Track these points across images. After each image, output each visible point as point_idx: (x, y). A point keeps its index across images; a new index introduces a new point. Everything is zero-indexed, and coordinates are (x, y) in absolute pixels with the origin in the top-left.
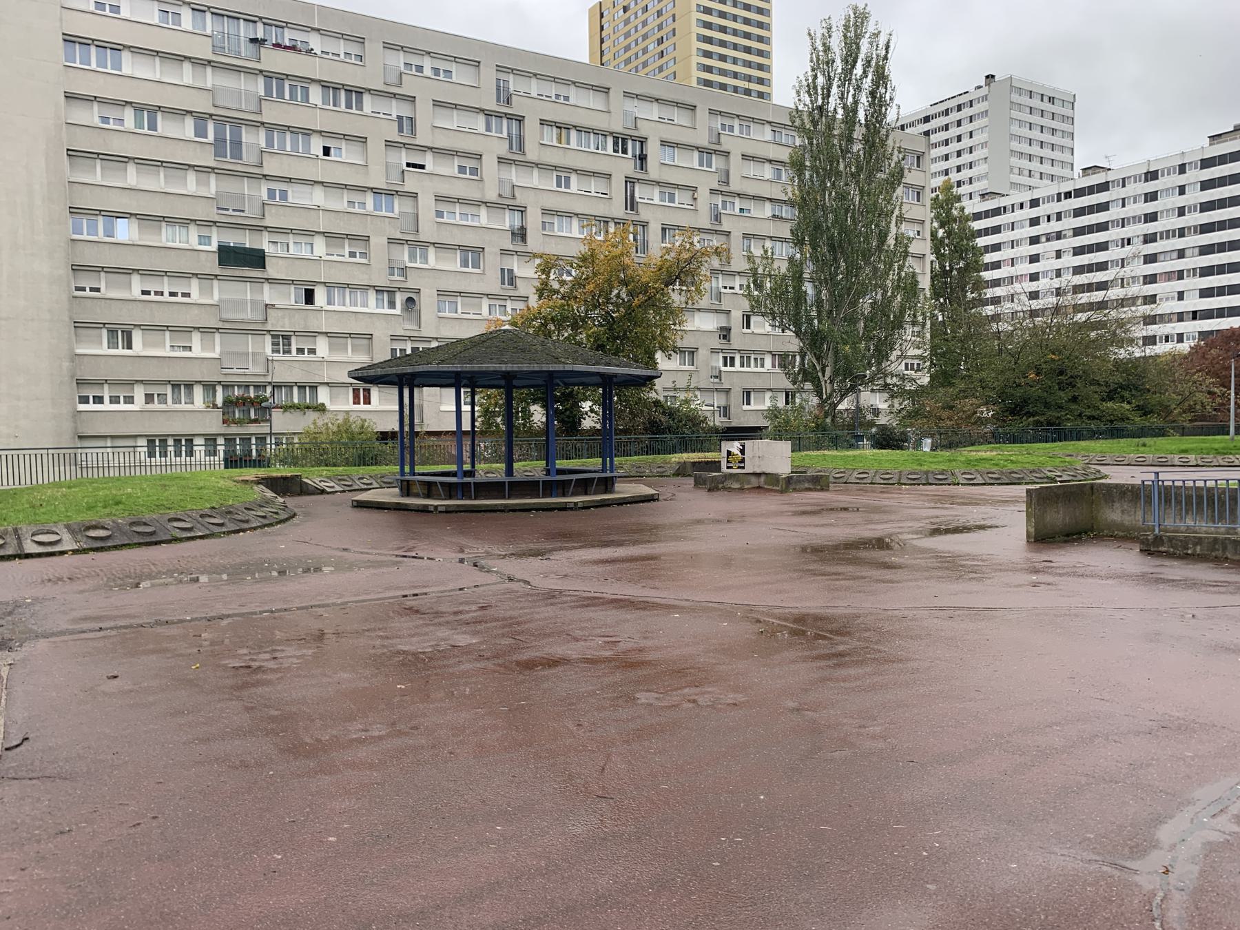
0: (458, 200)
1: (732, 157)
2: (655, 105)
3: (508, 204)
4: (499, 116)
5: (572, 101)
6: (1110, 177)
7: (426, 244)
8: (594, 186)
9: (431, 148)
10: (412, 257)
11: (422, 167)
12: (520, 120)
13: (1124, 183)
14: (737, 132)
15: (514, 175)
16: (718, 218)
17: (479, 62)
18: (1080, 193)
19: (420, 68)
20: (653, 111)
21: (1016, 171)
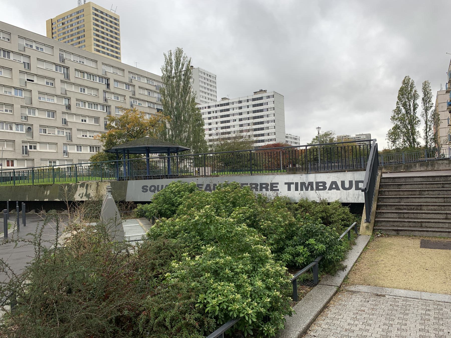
0: (47, 94)
1: (136, 87)
2: (112, 68)
3: (64, 96)
4: (60, 66)
5: (85, 64)
6: (230, 101)
7: (34, 109)
8: (93, 92)
9: (36, 75)
10: (29, 113)
11: (33, 81)
12: (68, 68)
13: (233, 103)
14: (137, 79)
15: (66, 87)
16: (132, 106)
17: (53, 47)
18: (222, 105)
19: (31, 46)
20: (111, 70)
21: (202, 97)
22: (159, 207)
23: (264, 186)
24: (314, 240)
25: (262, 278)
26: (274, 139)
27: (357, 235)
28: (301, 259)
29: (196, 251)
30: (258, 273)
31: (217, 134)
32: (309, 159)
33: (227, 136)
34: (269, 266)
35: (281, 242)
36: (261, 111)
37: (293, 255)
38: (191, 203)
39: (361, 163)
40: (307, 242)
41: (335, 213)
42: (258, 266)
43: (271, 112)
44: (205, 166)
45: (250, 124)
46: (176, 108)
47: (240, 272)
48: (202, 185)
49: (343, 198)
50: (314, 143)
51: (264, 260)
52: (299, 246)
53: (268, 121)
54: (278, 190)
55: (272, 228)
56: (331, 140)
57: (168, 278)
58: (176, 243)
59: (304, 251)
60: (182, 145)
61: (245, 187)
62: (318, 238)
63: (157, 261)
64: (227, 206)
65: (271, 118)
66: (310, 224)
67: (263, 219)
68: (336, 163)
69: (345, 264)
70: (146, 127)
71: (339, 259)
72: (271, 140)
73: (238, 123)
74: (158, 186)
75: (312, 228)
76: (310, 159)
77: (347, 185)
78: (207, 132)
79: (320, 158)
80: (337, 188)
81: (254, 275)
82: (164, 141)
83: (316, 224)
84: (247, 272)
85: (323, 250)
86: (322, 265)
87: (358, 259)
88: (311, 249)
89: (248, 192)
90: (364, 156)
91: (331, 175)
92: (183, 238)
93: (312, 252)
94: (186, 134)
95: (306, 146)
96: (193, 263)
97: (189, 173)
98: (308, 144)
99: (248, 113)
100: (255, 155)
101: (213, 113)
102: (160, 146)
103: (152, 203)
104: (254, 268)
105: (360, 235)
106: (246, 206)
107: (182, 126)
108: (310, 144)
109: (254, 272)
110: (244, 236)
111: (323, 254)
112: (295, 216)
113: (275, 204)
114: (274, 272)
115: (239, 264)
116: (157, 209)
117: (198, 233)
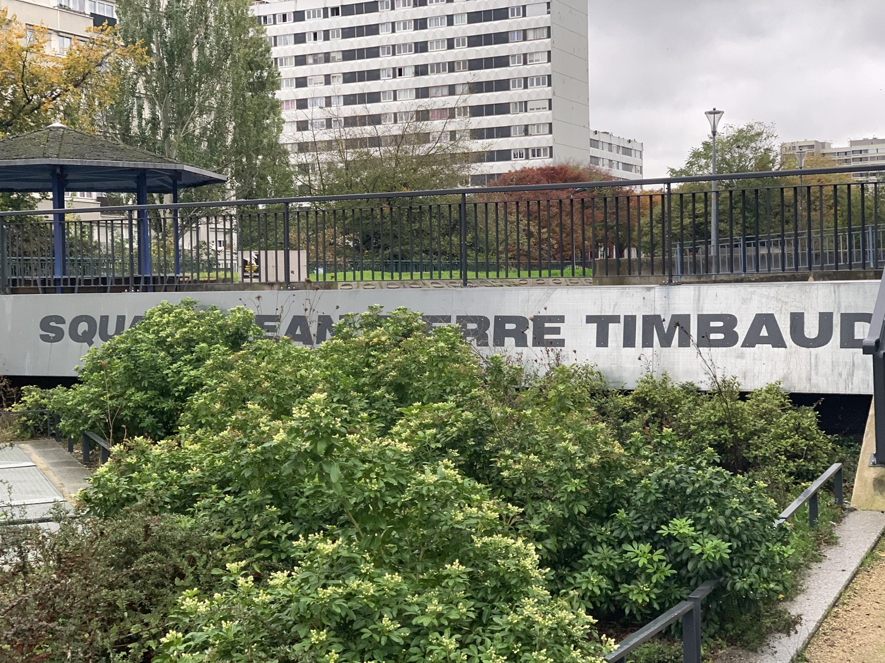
22: (111, 398)
23: (510, 326)
24: (690, 521)
25: (508, 648)
26: (545, 149)
27: (841, 512)
28: (641, 592)
29: (263, 558)
30: (493, 632)
31: (329, 124)
32: (676, 230)
33: (368, 131)
34: (533, 606)
35: (573, 530)
36: (502, 38)
37: (611, 578)
38: (238, 386)
39: (864, 246)
40: (664, 531)
41: (765, 430)
42: (493, 607)
43: (537, 44)
44: (287, 246)
45: (459, 89)
46: (169, 17)
47: (432, 628)
48: (276, 318)
49: (795, 377)
50: (695, 171)
51: (515, 586)
52: (635, 544)
53: (526, 79)
54: (561, 343)
55: (541, 479)
56: (764, 160)
57: (172, 649)
58: (191, 529)
59: (651, 561)
60: (197, 165)
61: (441, 330)
62: (703, 515)
63: (123, 593)
64: (375, 399)
65: (539, 67)
66: (677, 467)
67: (511, 445)
68: (776, 245)
69: (794, 610)
70: (51, 87)
71: (775, 591)
72: (536, 152)
73: (409, 81)
74: (105, 319)
75: (682, 480)
76: (683, 228)
77: (811, 330)
78: (290, 114)
79: (717, 226)
80: (777, 341)
81: (479, 640)
82: (122, 145)
83: (699, 467)
84: (456, 628)
85: (721, 557)
86: (717, 613)
87: (841, 595)
88: (677, 555)
89: (453, 348)
90: (876, 222)
91: (753, 293)
92: (215, 512)
93: (679, 565)
94: (208, 119)
95: (668, 182)
96: (263, 597)
97: (218, 270)
98: (672, 171)
99: (451, 44)
100: (481, 208)
101: (315, 38)
102: (109, 163)
103: (80, 383)
104: (480, 615)
105: (853, 510)
106: (446, 401)
107: (192, 89)
108: (682, 171)
109: (480, 629)
110: (445, 502)
111: (719, 573)
112: (621, 436)
113: (552, 393)
114: (551, 629)
115: (430, 600)
116: (101, 405)
117: (272, 492)
